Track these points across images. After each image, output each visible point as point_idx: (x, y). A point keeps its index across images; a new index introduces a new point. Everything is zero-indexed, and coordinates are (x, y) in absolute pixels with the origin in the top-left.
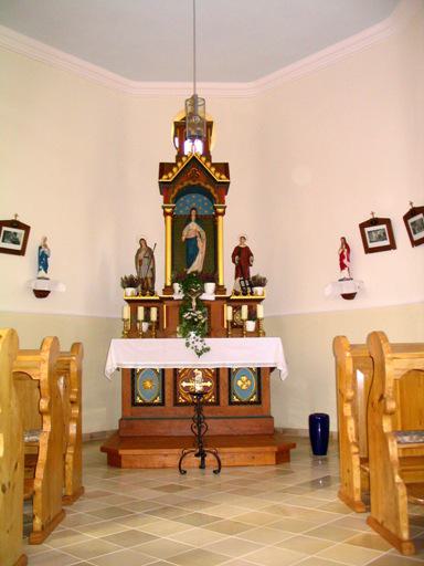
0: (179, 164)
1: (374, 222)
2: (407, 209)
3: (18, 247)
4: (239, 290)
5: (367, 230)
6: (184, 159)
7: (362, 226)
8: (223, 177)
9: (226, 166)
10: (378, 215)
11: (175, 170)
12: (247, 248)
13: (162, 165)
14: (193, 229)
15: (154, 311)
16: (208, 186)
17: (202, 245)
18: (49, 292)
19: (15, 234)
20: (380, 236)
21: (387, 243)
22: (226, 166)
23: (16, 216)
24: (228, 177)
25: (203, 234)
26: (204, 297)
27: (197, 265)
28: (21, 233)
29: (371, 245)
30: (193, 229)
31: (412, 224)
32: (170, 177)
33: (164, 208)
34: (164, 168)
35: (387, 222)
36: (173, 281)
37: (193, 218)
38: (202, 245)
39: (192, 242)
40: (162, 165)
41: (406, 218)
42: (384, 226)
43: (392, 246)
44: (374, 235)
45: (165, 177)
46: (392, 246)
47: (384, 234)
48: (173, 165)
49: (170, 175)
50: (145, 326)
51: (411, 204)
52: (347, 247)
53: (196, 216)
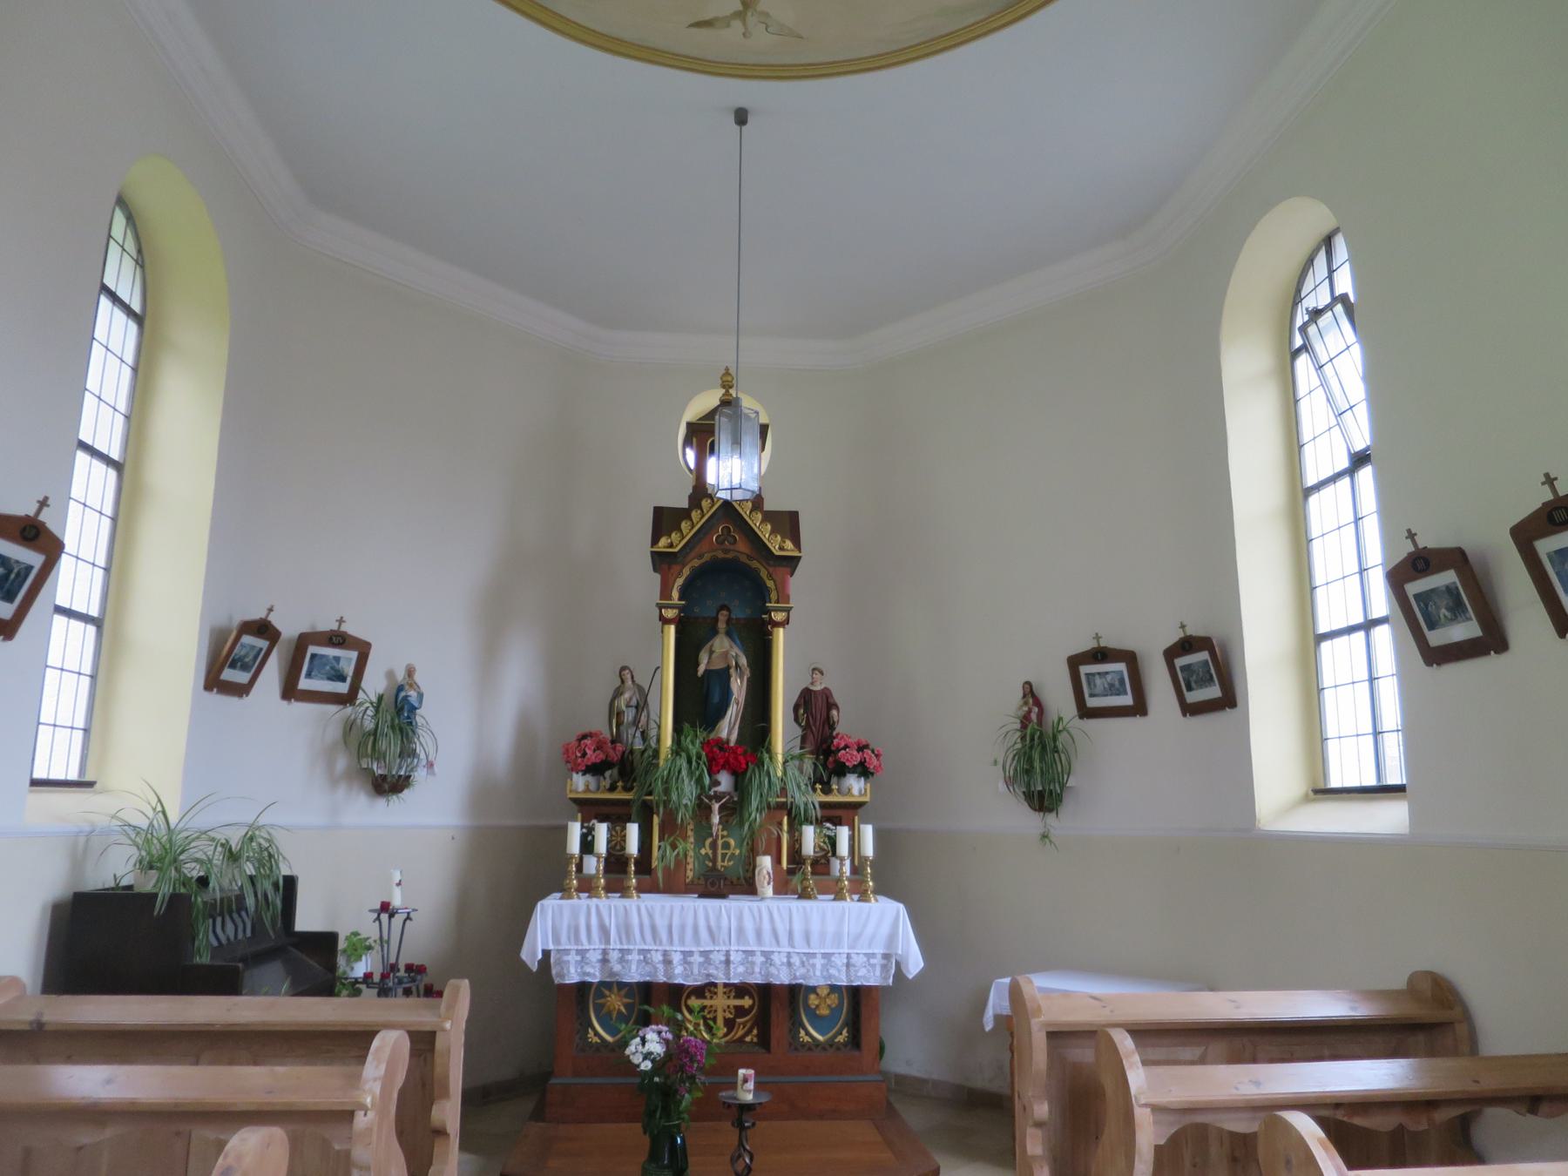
0: (695, 515)
1: (1100, 655)
2: (1174, 637)
3: (343, 688)
4: (377, 978)
5: (1084, 670)
6: (705, 503)
7: (1075, 662)
8: (789, 545)
9: (793, 517)
10: (1110, 642)
11: (684, 525)
12: (826, 693)
13: (659, 513)
14: (723, 650)
15: (633, 830)
16: (755, 564)
17: (738, 687)
18: (272, 607)
19: (337, 659)
20: (1111, 686)
21: (1127, 700)
22: (793, 517)
23: (341, 621)
24: (797, 543)
25: (743, 661)
26: (398, 974)
27: (728, 728)
28: (348, 658)
29: (1092, 703)
30: (723, 650)
31: (1183, 668)
32: (673, 542)
33: (660, 607)
34: (664, 520)
35: (1130, 658)
36: (454, 968)
37: (722, 626)
38: (738, 687)
39: (722, 677)
40: (659, 513)
41: (1171, 654)
42: (1121, 667)
43: (1139, 708)
44: (1098, 681)
45: (663, 541)
46: (1139, 708)
47: (1122, 681)
48: (684, 514)
49: (675, 536)
50: (592, 865)
51: (1183, 627)
52: (1037, 702)
53: (728, 622)
